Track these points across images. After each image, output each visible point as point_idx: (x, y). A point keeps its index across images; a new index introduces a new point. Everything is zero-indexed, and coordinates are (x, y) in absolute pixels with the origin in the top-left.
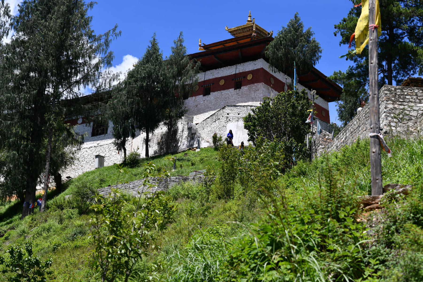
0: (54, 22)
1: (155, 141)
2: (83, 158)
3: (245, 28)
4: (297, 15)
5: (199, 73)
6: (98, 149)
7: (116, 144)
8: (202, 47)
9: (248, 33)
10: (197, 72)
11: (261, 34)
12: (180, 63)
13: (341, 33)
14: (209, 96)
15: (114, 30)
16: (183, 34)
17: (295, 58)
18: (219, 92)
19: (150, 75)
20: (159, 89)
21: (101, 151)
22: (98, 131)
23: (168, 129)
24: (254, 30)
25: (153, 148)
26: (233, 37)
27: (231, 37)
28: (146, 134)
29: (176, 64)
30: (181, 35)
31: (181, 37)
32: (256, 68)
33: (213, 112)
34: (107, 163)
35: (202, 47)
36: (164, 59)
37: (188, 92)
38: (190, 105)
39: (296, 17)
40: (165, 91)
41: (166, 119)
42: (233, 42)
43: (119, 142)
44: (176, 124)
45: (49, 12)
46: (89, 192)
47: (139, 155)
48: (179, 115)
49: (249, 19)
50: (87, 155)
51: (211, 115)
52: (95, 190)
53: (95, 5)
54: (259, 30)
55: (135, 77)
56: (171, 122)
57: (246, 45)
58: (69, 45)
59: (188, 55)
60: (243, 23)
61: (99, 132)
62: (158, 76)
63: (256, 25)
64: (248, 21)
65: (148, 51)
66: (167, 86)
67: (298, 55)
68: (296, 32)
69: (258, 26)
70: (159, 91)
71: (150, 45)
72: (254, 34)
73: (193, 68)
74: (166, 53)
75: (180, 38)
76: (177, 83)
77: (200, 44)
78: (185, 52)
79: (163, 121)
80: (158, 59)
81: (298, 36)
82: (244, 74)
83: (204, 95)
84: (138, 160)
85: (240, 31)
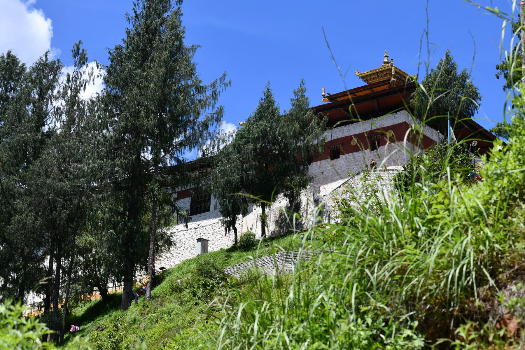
0: (157, 72)
1: (272, 218)
2: (180, 244)
3: (381, 72)
4: (449, 54)
5: (326, 130)
6: (199, 231)
7: (224, 223)
8: (326, 97)
9: (385, 78)
10: (324, 129)
11: (402, 78)
12: (303, 118)
13: (505, 74)
14: (338, 159)
15: (222, 79)
16: (305, 82)
17: (448, 107)
18: (351, 154)
19: (264, 134)
20: (277, 152)
21: (202, 234)
22: (197, 208)
23: (290, 202)
24: (393, 73)
25: (271, 227)
26: (366, 84)
27: (362, 83)
28: (261, 209)
29: (298, 119)
30: (302, 82)
31: (302, 85)
32: (397, 123)
33: (341, 182)
34: (213, 248)
35: (326, 97)
36: (282, 113)
37: (312, 156)
38: (314, 172)
39: (447, 56)
40: (283, 156)
41: (286, 190)
42: (367, 90)
43: (228, 219)
44: (299, 194)
45: (145, 59)
46: (212, 269)
47: (254, 236)
48: (303, 183)
49: (386, 60)
50: (184, 240)
51: (341, 183)
52: (219, 267)
53: (198, 48)
54: (400, 75)
55: (246, 138)
56: (292, 193)
57: (384, 94)
58: (173, 99)
59: (312, 108)
60: (378, 65)
61: (199, 209)
62: (275, 136)
63: (396, 68)
64: (385, 63)
65: (261, 104)
66: (286, 147)
67: (451, 104)
68: (448, 75)
69: (398, 69)
70: (277, 154)
71: (263, 97)
72: (392, 79)
73: (318, 124)
74: (284, 106)
75: (302, 87)
76: (298, 144)
77: (324, 94)
78: (308, 105)
79: (282, 192)
80: (274, 114)
81: (450, 80)
82: (348, 139)
83: (332, 159)
84: (253, 242)
85: (374, 76)
